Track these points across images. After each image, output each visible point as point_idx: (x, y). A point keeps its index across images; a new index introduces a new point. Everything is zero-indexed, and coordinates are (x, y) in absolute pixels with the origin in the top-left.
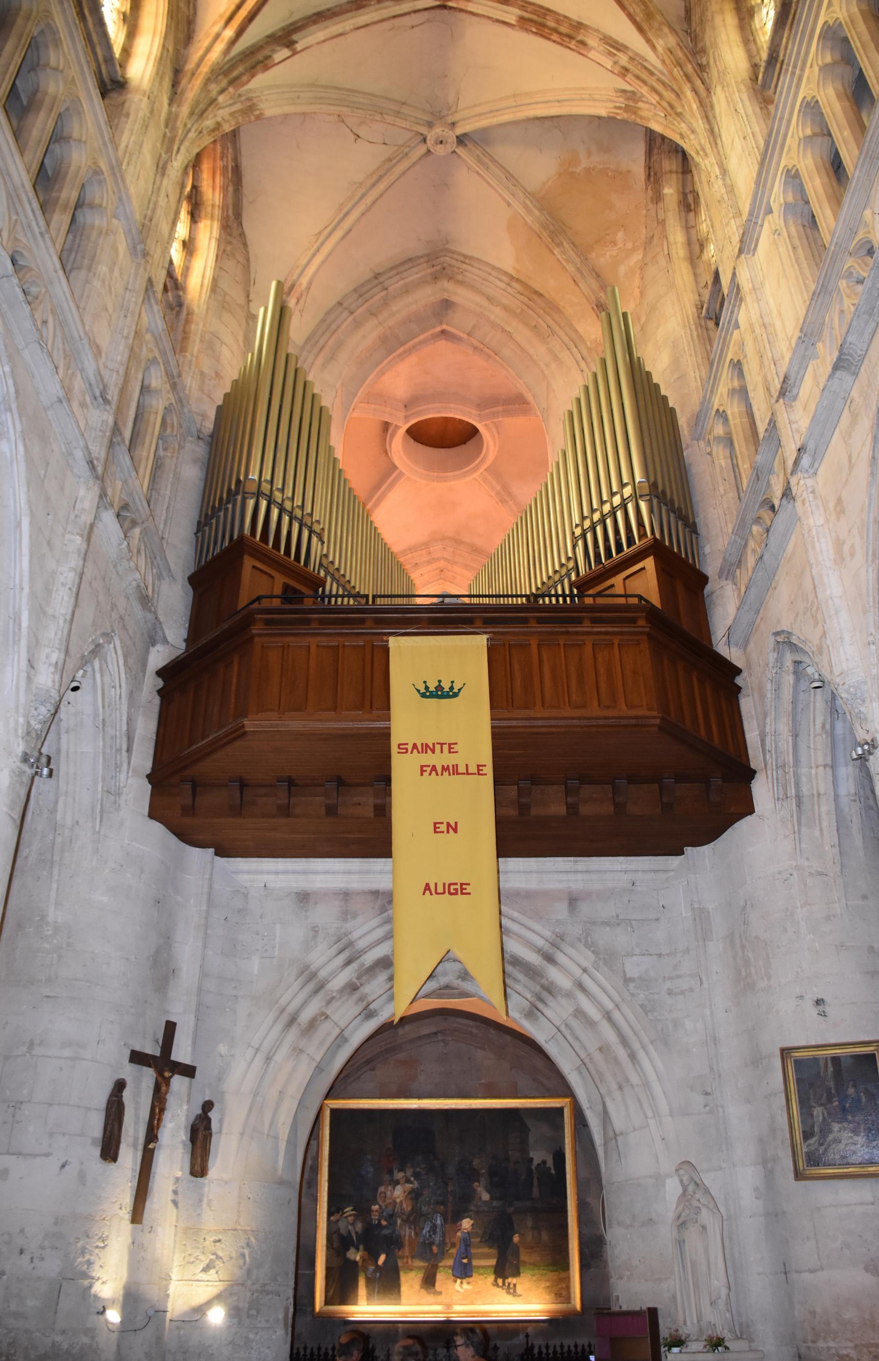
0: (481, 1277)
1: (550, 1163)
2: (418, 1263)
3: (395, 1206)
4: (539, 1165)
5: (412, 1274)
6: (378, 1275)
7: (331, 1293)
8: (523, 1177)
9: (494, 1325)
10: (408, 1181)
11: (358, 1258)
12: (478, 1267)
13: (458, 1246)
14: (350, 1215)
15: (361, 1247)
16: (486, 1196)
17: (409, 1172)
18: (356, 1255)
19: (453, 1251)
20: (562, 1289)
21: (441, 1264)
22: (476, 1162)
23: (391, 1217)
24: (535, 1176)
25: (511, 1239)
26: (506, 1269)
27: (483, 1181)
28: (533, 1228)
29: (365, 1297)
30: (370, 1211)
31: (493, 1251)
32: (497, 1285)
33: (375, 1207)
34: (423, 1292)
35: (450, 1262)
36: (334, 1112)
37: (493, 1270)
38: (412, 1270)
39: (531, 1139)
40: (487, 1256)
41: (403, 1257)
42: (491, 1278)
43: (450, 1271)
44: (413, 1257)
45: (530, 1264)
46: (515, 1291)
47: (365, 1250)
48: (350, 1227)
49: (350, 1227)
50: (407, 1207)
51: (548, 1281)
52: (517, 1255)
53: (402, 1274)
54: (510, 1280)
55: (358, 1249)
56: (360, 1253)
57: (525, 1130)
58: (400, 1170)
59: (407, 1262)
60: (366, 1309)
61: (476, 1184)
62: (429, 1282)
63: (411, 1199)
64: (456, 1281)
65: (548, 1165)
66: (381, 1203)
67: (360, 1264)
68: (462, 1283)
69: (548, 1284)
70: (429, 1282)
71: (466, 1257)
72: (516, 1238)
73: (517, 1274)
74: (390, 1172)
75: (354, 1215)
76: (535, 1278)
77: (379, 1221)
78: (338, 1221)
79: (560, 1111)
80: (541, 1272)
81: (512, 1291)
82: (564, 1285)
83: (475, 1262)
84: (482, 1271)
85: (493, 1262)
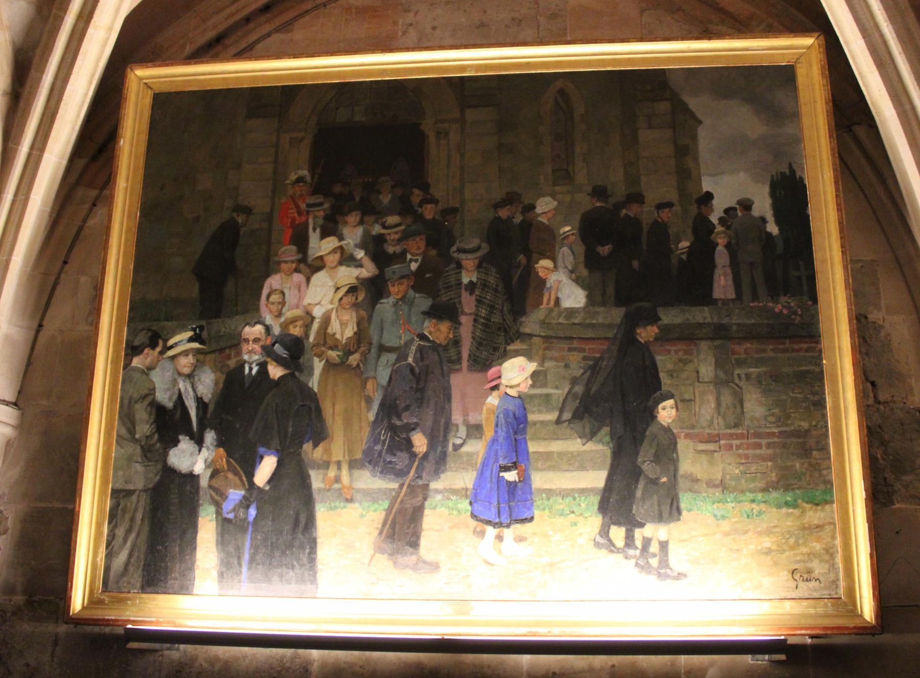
0: (559, 521)
1: (763, 206)
2: (368, 480)
3: (307, 327)
4: (726, 211)
5: (352, 512)
6: (253, 512)
7: (121, 559)
8: (685, 244)
9: (599, 661)
10: (347, 259)
11: (199, 468)
12: (550, 493)
13: (489, 433)
14: (185, 353)
15: (210, 437)
16: (574, 297)
17: (353, 235)
18: (193, 458)
19: (476, 448)
20: (811, 555)
21: (433, 485)
22: (545, 206)
23: (294, 351)
24: (721, 241)
25: (652, 416)
26: (634, 491)
27: (565, 254)
28: (718, 383)
29: (215, 574)
30: (236, 342)
31: (600, 449)
32: (610, 545)
33: (254, 331)
34: (383, 561)
35: (466, 479)
36: (165, 103)
37: (595, 500)
38: (350, 500)
39: (705, 142)
40: (580, 463)
41: (326, 465)
42: (595, 521)
43: (465, 505)
44: (354, 465)
45: (711, 484)
46: (664, 562)
47: (220, 443)
48: (182, 385)
49: (182, 385)
50: (344, 328)
51: (768, 532)
52: (666, 453)
53: (322, 513)
54: (649, 530)
55: (199, 441)
56: (205, 453)
57: (683, 123)
58: (325, 233)
59: (337, 480)
60: (214, 596)
61: (545, 263)
62: (402, 530)
63: (355, 306)
64: (482, 534)
65: (756, 212)
66: (269, 320)
67: (204, 482)
68: (500, 538)
69: (767, 542)
70: (402, 530)
71: (515, 466)
72: (666, 412)
73: (670, 510)
74: (301, 242)
75: (197, 352)
76: (726, 526)
77: (263, 366)
78: (151, 368)
79: (784, 75)
80: (747, 506)
81: (656, 560)
82: (817, 546)
83: (539, 480)
84: (561, 504)
85: (597, 479)
